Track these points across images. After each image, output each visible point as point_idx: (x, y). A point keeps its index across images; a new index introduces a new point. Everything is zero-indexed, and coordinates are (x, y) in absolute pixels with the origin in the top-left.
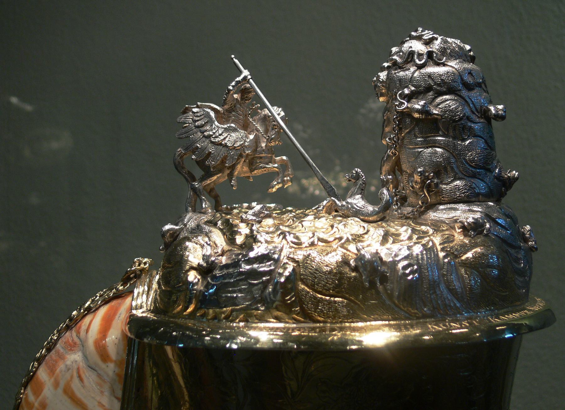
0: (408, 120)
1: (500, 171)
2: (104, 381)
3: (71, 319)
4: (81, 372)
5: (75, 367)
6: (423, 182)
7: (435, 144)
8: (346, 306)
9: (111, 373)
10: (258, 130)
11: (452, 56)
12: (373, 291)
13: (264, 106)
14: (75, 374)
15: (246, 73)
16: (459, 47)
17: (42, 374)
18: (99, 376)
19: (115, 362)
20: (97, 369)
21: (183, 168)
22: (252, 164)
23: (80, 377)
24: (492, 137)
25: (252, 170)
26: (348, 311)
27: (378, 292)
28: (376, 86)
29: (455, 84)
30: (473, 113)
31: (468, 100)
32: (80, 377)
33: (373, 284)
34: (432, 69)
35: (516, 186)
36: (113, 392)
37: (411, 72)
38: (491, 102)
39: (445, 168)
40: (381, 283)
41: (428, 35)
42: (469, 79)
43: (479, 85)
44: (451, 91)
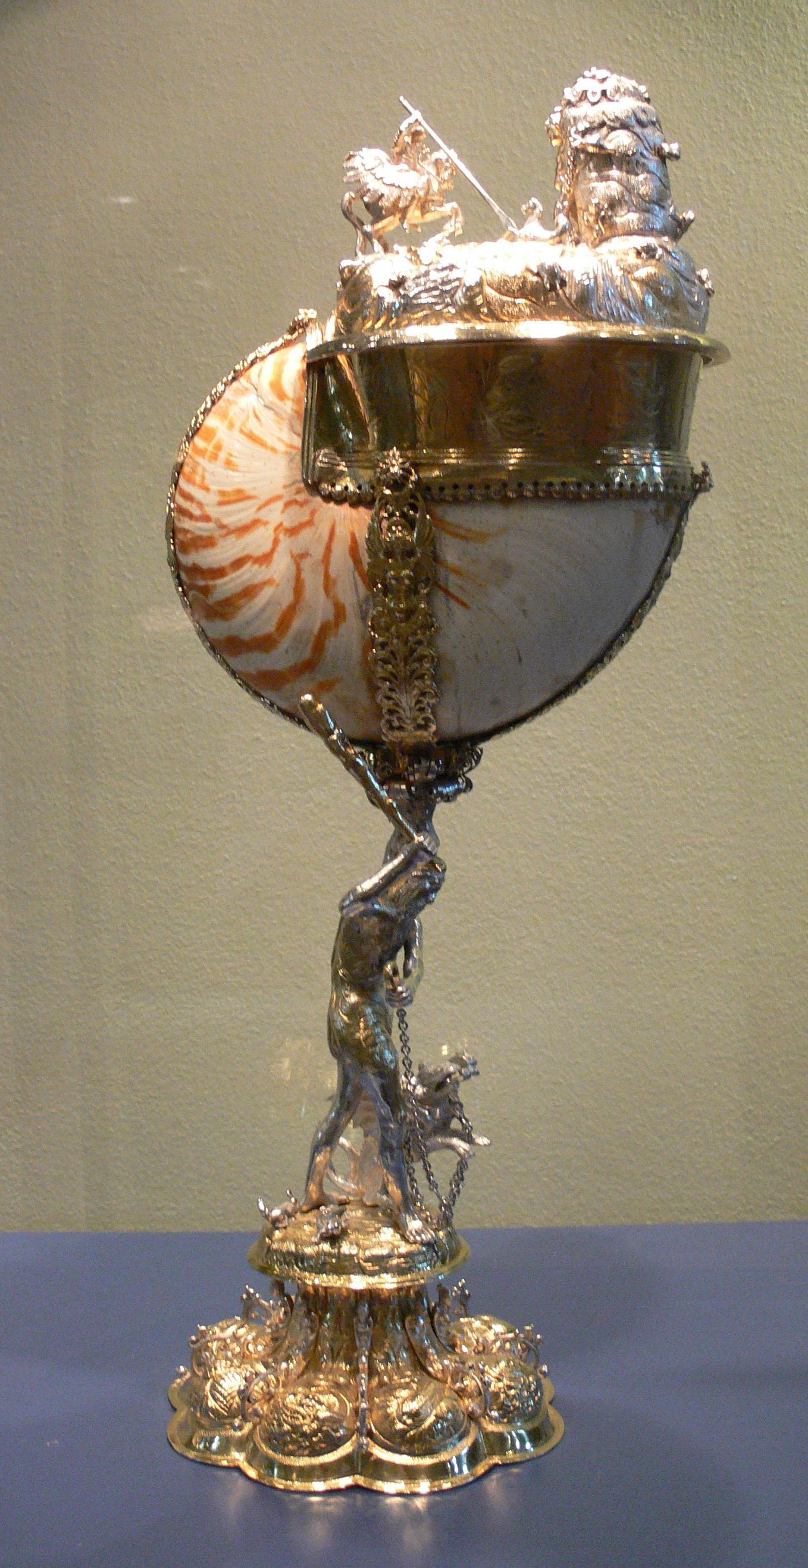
0: (582, 156)
1: (675, 210)
2: (282, 418)
3: (235, 371)
4: (258, 413)
5: (251, 408)
6: (598, 214)
7: (607, 179)
8: (530, 307)
9: (289, 411)
10: (428, 173)
11: (625, 94)
12: (554, 293)
13: (439, 148)
14: (252, 415)
15: (416, 115)
16: (634, 88)
17: (211, 421)
18: (276, 413)
19: (293, 400)
20: (273, 407)
21: (351, 213)
22: (424, 209)
23: (257, 417)
24: (666, 176)
25: (423, 214)
26: (531, 312)
27: (558, 295)
28: (548, 129)
29: (627, 120)
30: (647, 149)
31: (641, 136)
32: (257, 417)
33: (553, 288)
34: (604, 105)
35: (693, 225)
36: (292, 428)
37: (583, 110)
38: (665, 141)
39: (619, 201)
40: (561, 287)
41: (602, 73)
42: (643, 117)
43: (653, 123)
44: (624, 126)
